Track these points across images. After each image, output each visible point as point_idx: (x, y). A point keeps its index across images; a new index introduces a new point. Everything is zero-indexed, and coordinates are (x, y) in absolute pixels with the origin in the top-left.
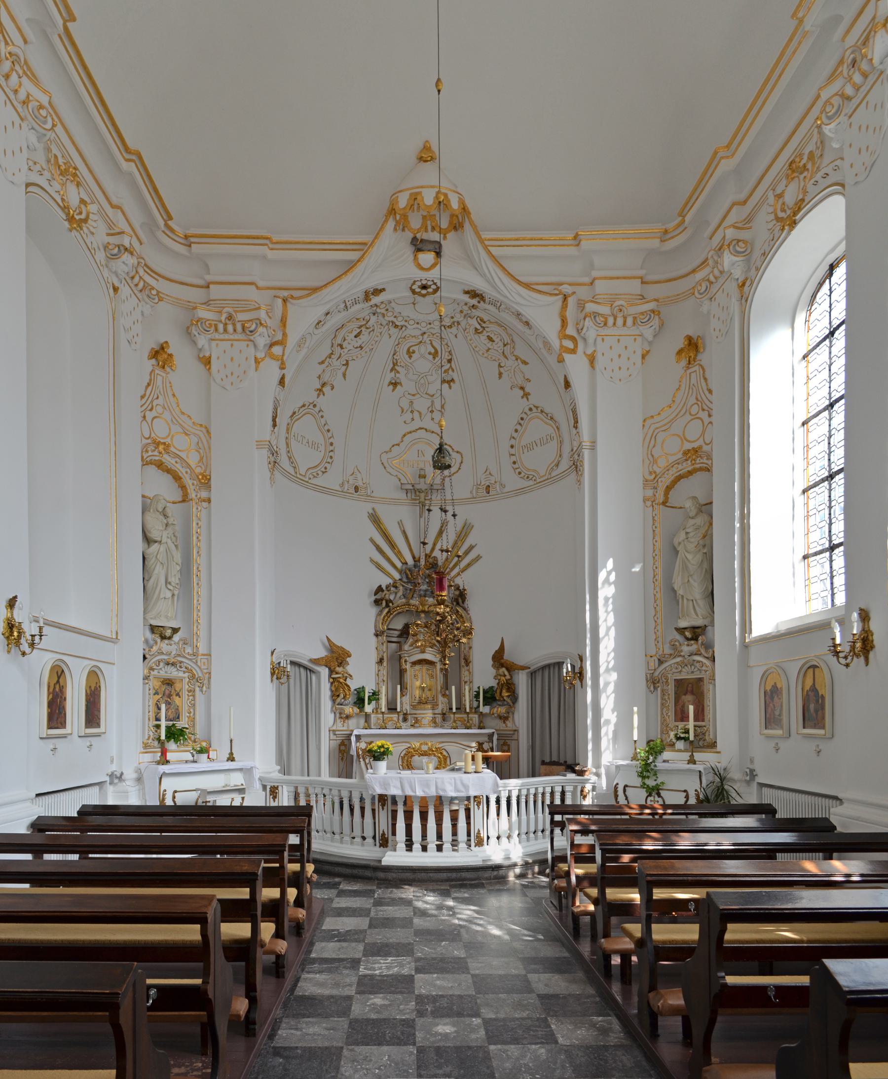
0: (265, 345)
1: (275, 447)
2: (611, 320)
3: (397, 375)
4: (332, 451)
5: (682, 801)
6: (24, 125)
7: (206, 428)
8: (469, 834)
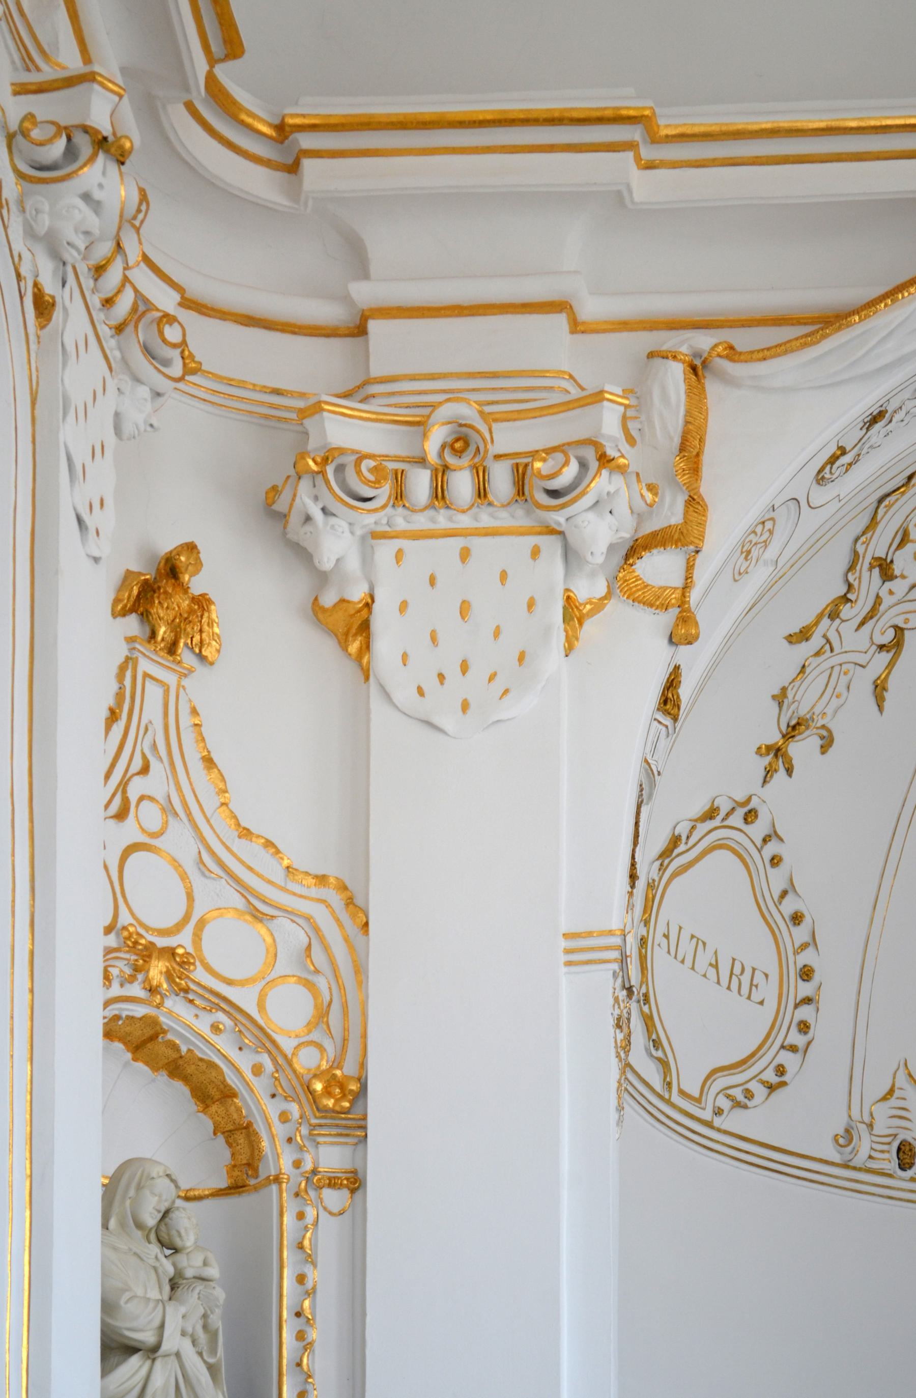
0: (612, 548)
4: (808, 1001)
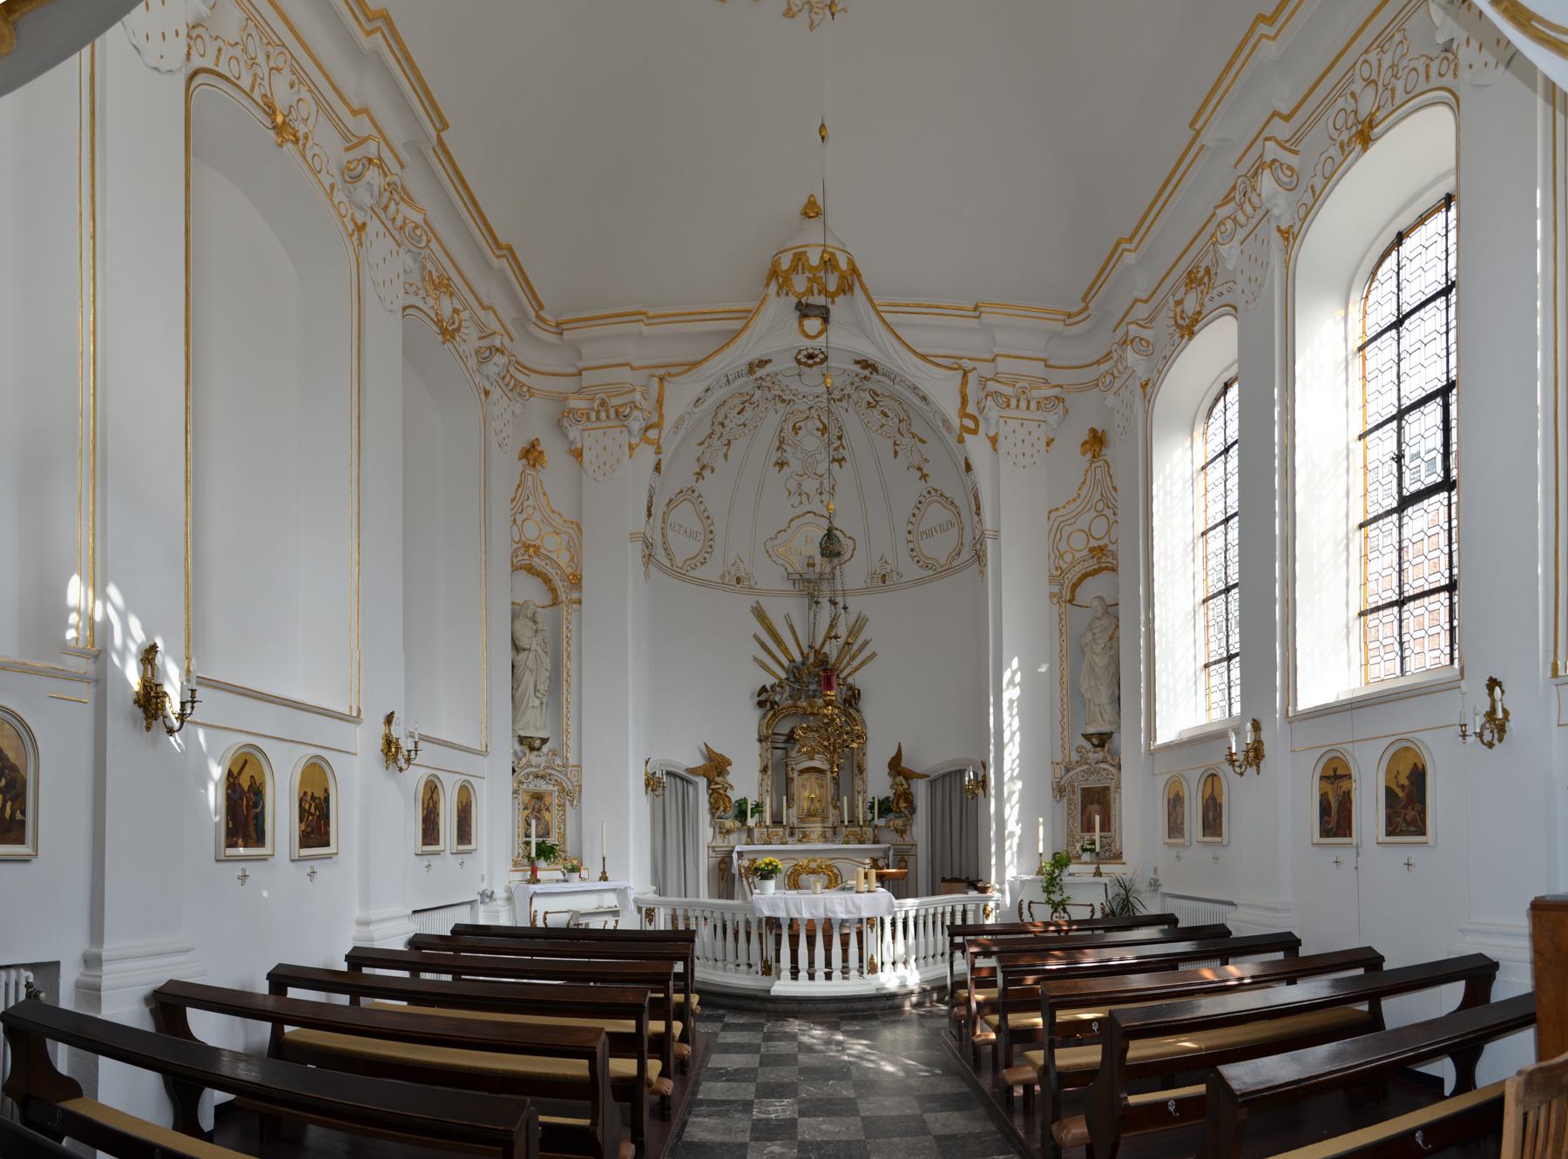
0: (640, 429)
1: (650, 539)
2: (1013, 403)
3: (784, 454)
5: (1087, 916)
6: (401, 250)
7: (577, 524)
8: (861, 960)
